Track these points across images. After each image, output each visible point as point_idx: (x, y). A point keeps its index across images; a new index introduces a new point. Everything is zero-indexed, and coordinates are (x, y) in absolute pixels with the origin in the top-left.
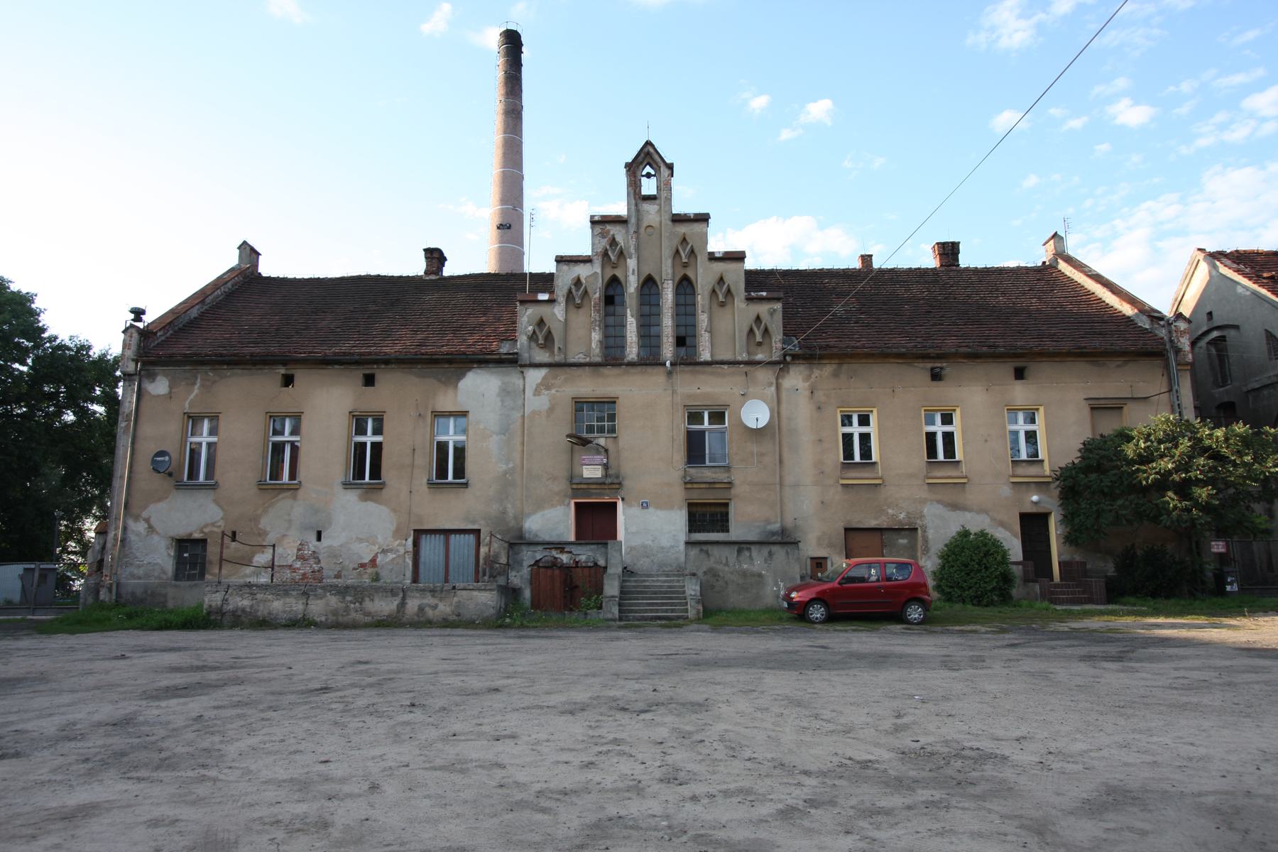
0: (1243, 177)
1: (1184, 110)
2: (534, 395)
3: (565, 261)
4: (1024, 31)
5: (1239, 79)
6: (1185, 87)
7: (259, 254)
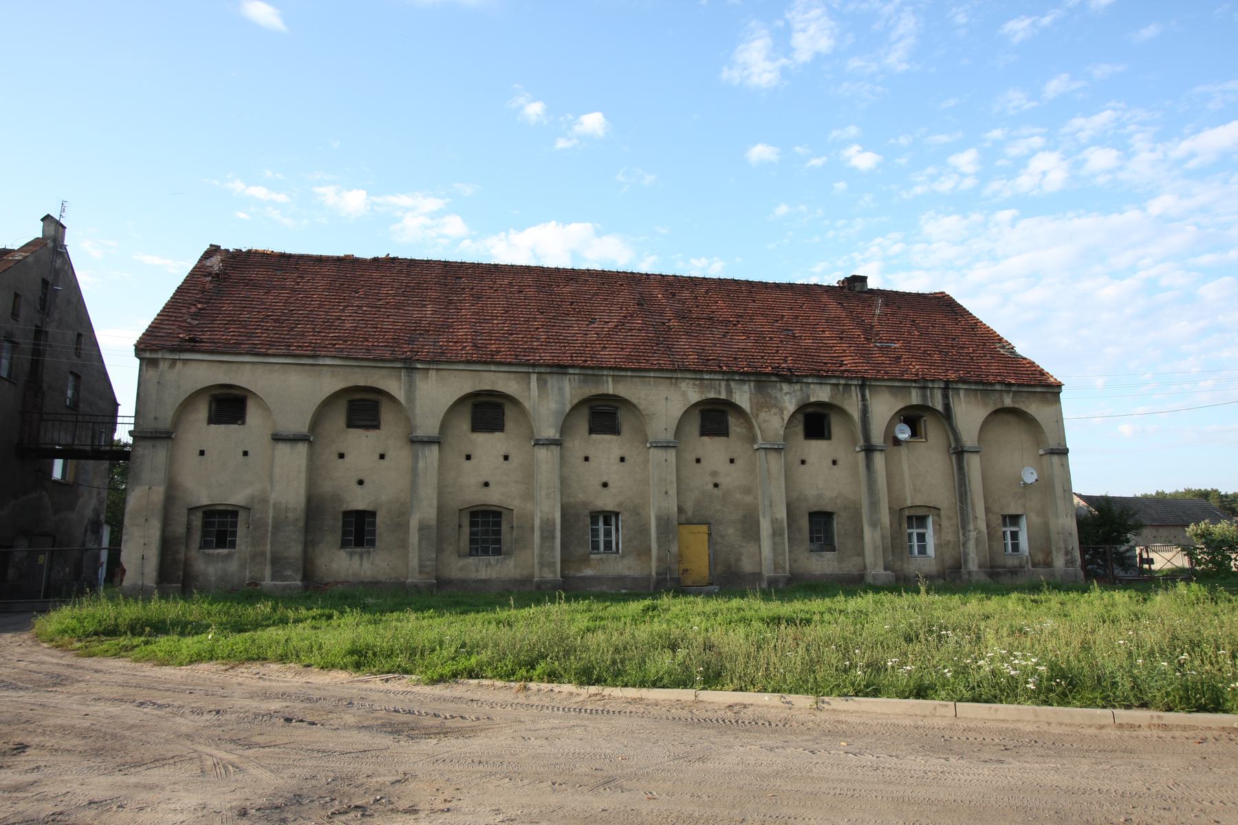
0: (952, 223)
1: (903, 161)
2: (710, 475)
3: (1057, 453)
4: (771, 72)
5: (943, 138)
6: (903, 141)
7: (64, 228)
